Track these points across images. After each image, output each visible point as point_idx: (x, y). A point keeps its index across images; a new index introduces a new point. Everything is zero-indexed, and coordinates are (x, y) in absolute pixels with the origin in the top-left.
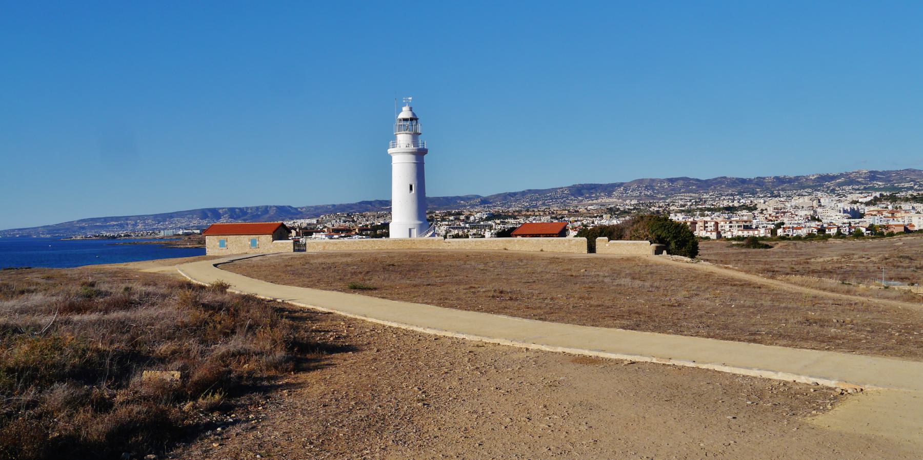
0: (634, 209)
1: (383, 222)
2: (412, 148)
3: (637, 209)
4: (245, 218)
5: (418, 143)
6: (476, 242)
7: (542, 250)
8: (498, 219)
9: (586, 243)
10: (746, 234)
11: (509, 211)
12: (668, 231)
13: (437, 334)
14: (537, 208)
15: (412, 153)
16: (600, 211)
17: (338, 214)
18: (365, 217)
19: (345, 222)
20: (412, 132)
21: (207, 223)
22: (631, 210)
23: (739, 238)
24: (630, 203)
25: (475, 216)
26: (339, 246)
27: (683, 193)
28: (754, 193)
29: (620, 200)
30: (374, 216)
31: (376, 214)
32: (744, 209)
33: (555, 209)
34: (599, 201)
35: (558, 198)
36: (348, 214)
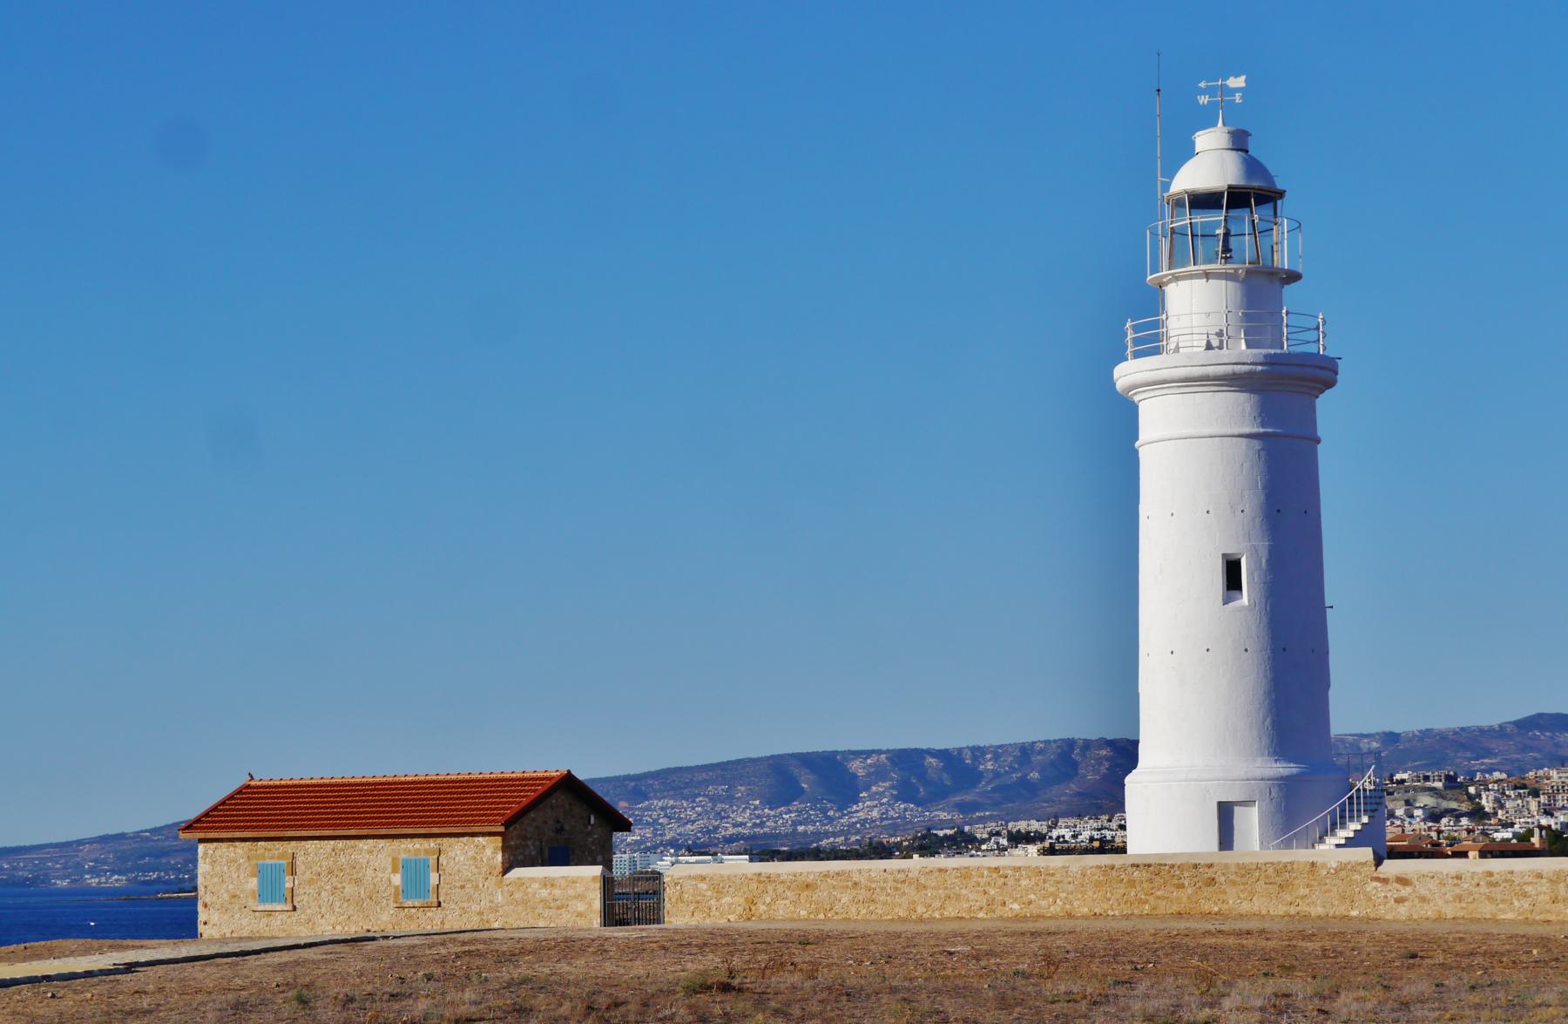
4: (968, 798)
15: (1234, 381)
17: (1398, 777)
18: (1535, 793)
19: (1434, 816)
21: (795, 823)
36: (1451, 780)
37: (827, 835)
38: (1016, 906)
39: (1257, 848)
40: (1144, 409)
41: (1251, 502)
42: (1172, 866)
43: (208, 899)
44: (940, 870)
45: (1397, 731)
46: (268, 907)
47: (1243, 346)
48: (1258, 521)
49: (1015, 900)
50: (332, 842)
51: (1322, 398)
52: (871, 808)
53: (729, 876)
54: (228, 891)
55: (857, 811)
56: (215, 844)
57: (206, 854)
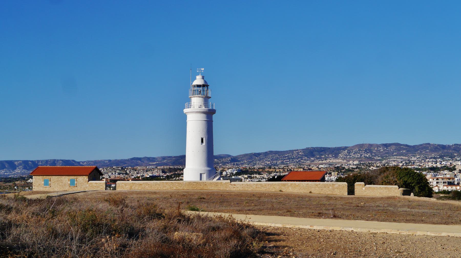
0: (356, 168)
1: (151, 175)
2: (203, 109)
3: (359, 168)
5: (208, 105)
6: (257, 185)
7: (310, 192)
8: (246, 175)
9: (347, 186)
10: (450, 188)
11: (254, 168)
12: (413, 178)
13: (326, 229)
14: (277, 165)
15: (204, 113)
16: (329, 169)
17: (113, 167)
18: (136, 171)
19: (119, 174)
20: (204, 96)
21: (4, 173)
22: (354, 168)
23: (444, 192)
24: (353, 164)
25: (227, 171)
26: (143, 186)
27: (395, 155)
28: (452, 157)
29: (345, 161)
30: (143, 170)
31: (145, 168)
32: (445, 169)
33: (292, 167)
34: (328, 161)
35: (294, 158)
36: (122, 168)
37: (10, 175)
38: (175, 188)
39: (205, 180)
40: (188, 116)
41: (205, 130)
42: (200, 182)
43: (35, 185)
44: (163, 183)
45: (111, 160)
46: (46, 186)
47: (204, 107)
48: (206, 133)
49: (175, 187)
50: (58, 176)
51: (214, 115)
52: (18, 171)
53: (127, 183)
54: (38, 184)
55: (16, 171)
56: (36, 176)
57: (34, 178)
